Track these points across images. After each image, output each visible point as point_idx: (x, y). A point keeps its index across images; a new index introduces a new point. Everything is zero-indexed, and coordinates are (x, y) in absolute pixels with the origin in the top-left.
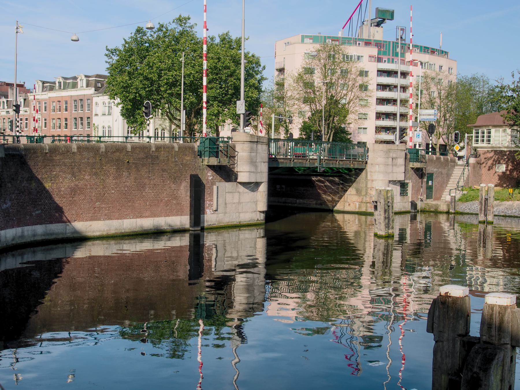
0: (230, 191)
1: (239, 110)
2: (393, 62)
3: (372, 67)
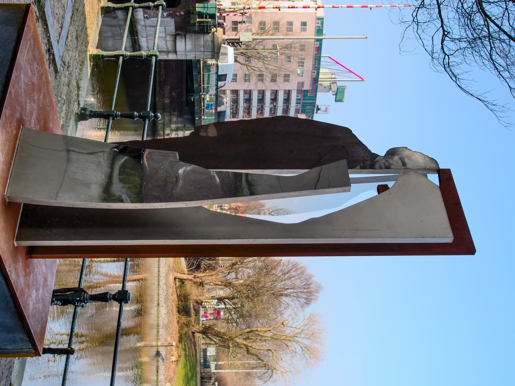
0: (167, 30)
1: (243, 35)
2: (297, 103)
3: (293, 86)
